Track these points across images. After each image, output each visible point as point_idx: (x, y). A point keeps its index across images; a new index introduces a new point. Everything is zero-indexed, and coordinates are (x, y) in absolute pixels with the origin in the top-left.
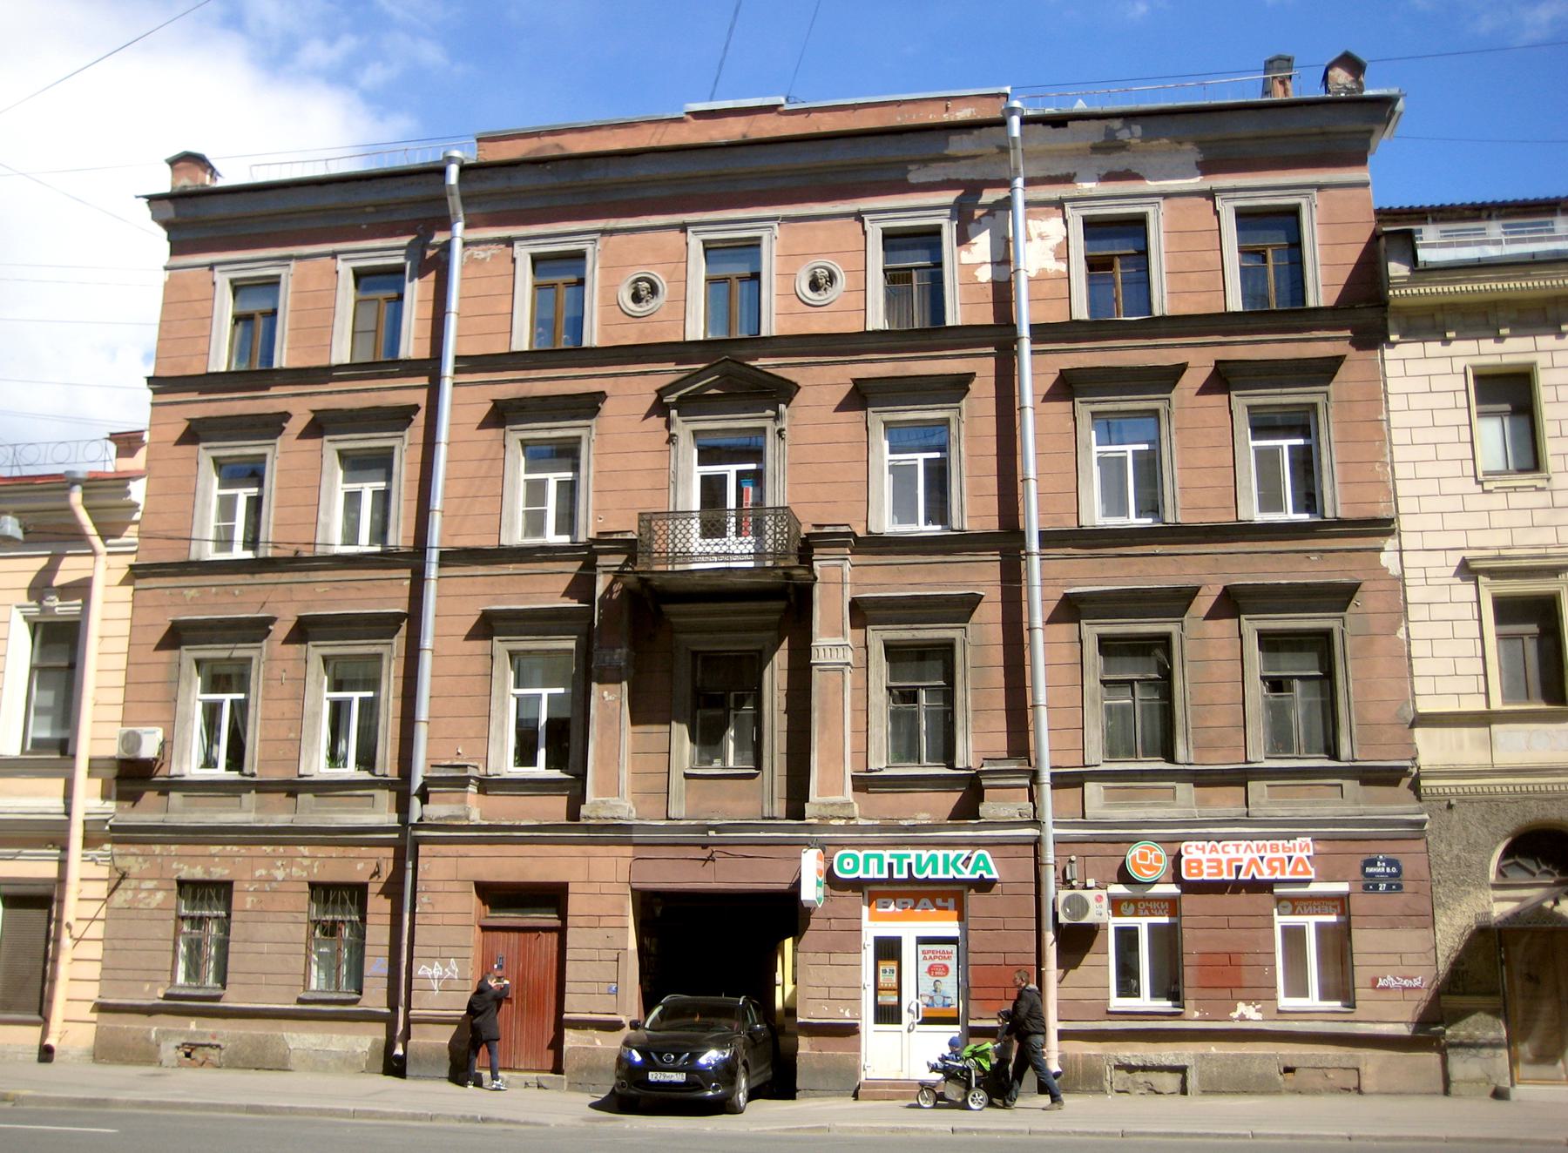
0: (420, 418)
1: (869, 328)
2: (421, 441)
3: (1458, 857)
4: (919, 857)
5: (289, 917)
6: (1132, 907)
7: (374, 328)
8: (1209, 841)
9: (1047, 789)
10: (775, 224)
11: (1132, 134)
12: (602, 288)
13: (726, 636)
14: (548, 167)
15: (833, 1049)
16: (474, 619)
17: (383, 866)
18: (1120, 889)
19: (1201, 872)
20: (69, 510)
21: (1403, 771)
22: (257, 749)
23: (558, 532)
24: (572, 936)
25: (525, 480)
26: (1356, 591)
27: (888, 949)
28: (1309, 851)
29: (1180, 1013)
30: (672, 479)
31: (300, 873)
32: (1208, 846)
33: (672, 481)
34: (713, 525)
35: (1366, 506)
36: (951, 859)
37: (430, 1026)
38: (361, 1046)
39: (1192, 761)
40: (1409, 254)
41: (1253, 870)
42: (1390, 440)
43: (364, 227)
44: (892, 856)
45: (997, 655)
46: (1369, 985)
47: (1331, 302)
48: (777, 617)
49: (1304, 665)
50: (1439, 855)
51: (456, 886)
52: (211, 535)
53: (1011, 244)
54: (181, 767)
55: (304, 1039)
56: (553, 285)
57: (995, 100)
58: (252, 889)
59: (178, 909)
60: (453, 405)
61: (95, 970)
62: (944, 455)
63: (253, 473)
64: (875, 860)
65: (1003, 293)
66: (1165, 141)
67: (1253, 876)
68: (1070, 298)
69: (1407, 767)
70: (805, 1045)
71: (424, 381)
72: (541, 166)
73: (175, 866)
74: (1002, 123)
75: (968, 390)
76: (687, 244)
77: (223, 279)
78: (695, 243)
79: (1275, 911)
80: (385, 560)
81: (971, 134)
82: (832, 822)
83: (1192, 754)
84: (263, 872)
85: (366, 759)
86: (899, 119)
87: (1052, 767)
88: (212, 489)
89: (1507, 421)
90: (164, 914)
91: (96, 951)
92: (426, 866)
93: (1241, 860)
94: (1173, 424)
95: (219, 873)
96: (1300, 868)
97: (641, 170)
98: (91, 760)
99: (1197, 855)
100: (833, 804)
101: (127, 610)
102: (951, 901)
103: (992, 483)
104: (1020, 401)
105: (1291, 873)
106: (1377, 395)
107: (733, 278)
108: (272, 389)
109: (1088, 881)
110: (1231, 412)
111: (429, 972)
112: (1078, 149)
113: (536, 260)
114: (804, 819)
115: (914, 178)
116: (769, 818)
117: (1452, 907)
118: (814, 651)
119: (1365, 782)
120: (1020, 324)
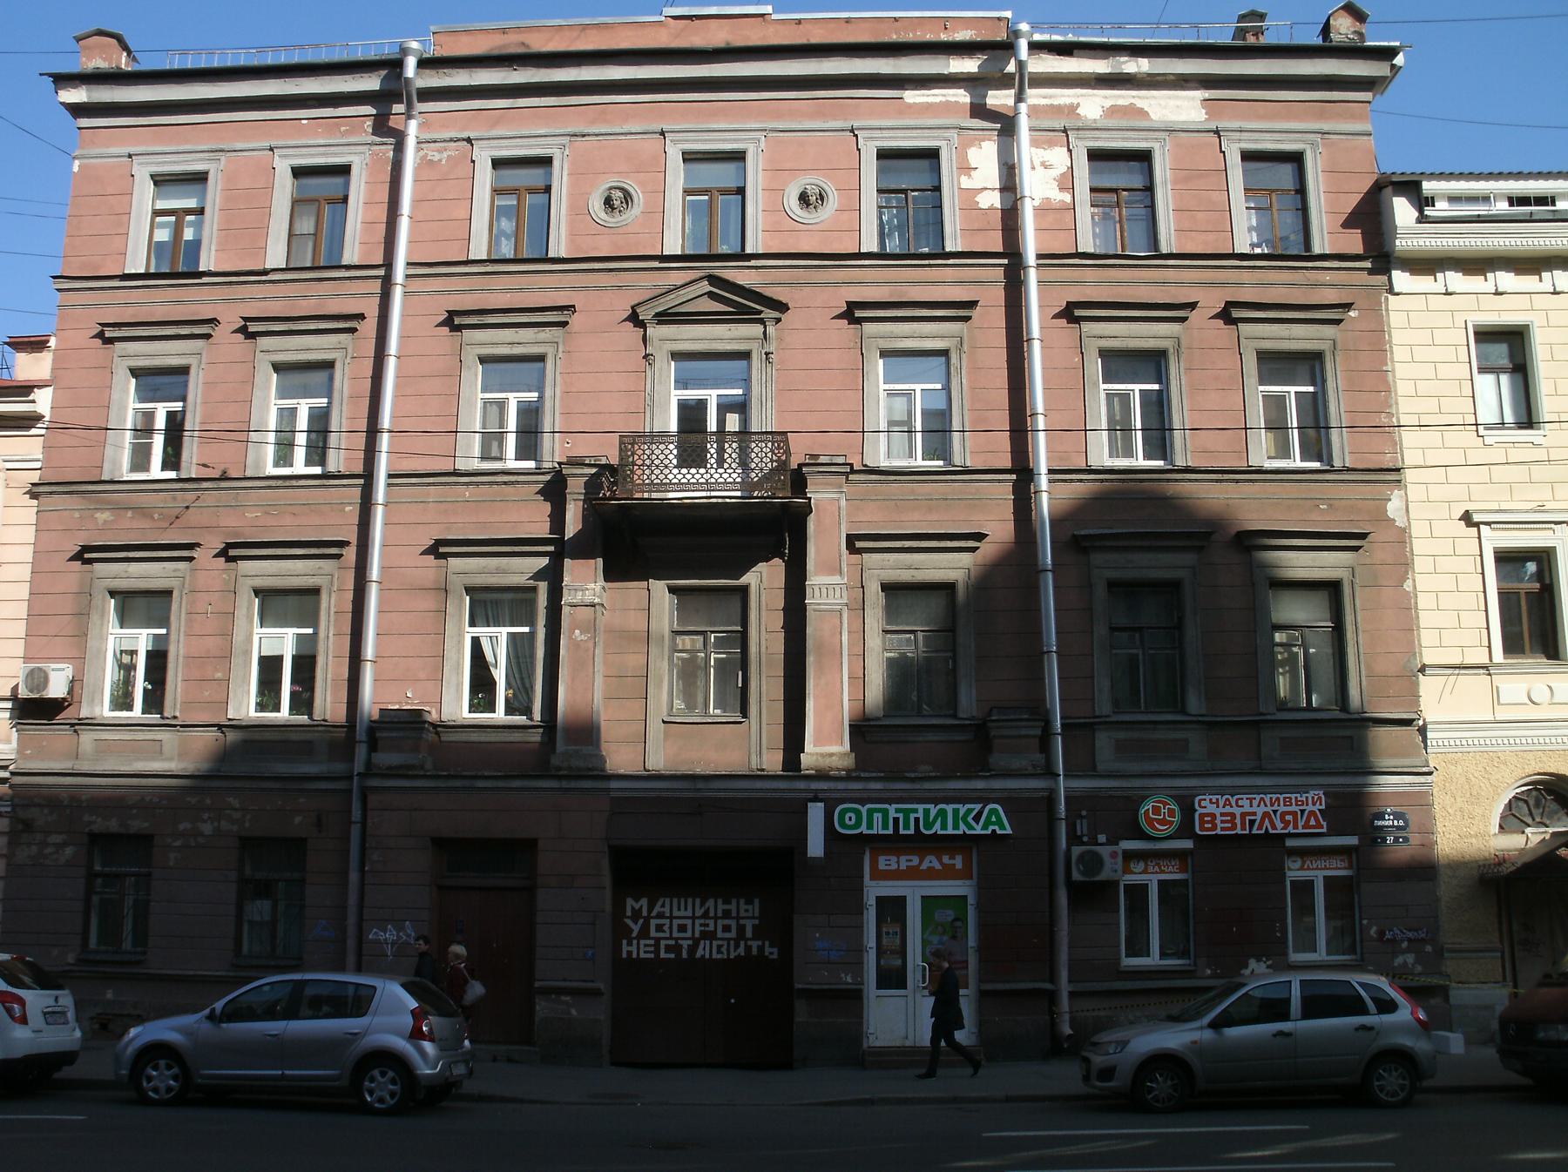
4: (927, 812)
8: (1232, 796)
19: (1215, 827)
22: (179, 690)
28: (1321, 804)
30: (648, 402)
33: (648, 404)
44: (897, 811)
64: (880, 815)
70: (802, 1013)
75: (1146, 112)
86: (895, 37)
89: (1504, 378)
93: (1254, 814)
94: (1182, 364)
96: (1312, 822)
99: (1211, 809)
104: (1027, 334)
105: (1304, 827)
111: (382, 936)
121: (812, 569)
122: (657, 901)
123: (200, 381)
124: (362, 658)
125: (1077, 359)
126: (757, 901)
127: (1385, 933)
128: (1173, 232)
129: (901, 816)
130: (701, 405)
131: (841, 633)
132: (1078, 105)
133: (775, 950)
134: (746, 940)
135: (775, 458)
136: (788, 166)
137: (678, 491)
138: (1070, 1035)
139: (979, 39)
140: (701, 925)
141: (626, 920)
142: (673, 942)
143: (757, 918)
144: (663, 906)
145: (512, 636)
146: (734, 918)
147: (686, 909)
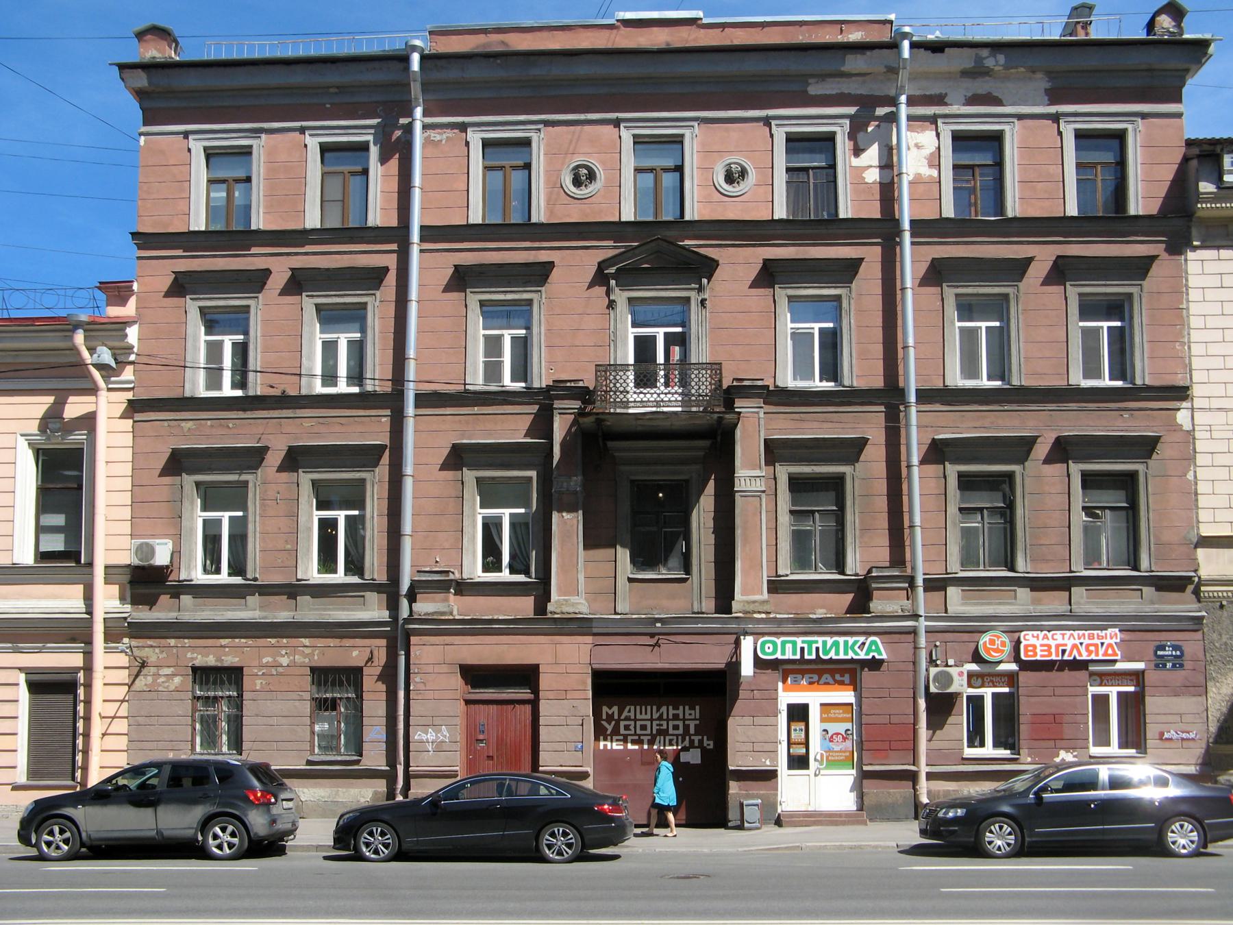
0: (391, 279)
1: (776, 217)
2: (394, 298)
3: (1226, 644)
4: (825, 643)
5: (294, 696)
6: (980, 680)
7: (341, 198)
8: (1042, 631)
9: (920, 590)
10: (696, 124)
11: (995, 62)
12: (546, 172)
13: (659, 468)
14: (499, 61)
15: (759, 788)
16: (446, 452)
17: (375, 653)
18: (974, 667)
19: (1035, 654)
20: (74, 350)
21: (1189, 579)
23: (514, 379)
24: (543, 705)
25: (205, 341)
26: (1158, 442)
27: (799, 713)
28: (1117, 638)
29: (1017, 759)
30: (612, 338)
31: (302, 660)
32: (1041, 634)
33: (613, 340)
34: (645, 376)
35: (1168, 377)
36: (850, 644)
37: (428, 780)
38: (363, 797)
39: (1029, 570)
40: (1216, 174)
41: (1075, 652)
42: (1189, 325)
43: (328, 106)
44: (803, 642)
45: (882, 486)
46: (1157, 737)
47: (1153, 209)
48: (703, 453)
49: (1116, 498)
50: (1212, 642)
51: (445, 669)
52: (318, 370)
53: (895, 151)
54: (189, 573)
55: (315, 793)
56: (502, 168)
57: (881, 26)
58: (260, 673)
59: (193, 691)
60: (421, 268)
61: (122, 743)
62: (685, 330)
63: (237, 320)
65: (888, 192)
66: (1022, 69)
67: (1075, 657)
68: (940, 199)
69: (1192, 577)
71: (394, 247)
72: (492, 60)
73: (189, 655)
74: (894, 46)
76: (620, 137)
77: (197, 147)
78: (627, 135)
79: (1089, 684)
80: (364, 400)
81: (864, 54)
82: (756, 616)
83: (1029, 565)
84: (270, 659)
85: (355, 565)
86: (801, 38)
87: (924, 574)
88: (200, 338)
90: (182, 696)
91: (121, 726)
92: (418, 653)
93: (1066, 645)
94: (1020, 306)
95: (230, 660)
96: (1110, 651)
97: (582, 69)
98: (106, 567)
99: (1033, 641)
100: (754, 602)
101: (128, 439)
102: (847, 678)
103: (878, 350)
105: (1103, 655)
106: (1179, 289)
107: (658, 169)
108: (253, 249)
109: (949, 661)
110: (1066, 298)
111: (424, 737)
112: (950, 73)
113: (487, 144)
114: (731, 613)
115: (814, 89)
116: (698, 613)
117: (1220, 680)
118: (736, 481)
119: (1159, 588)
120: (903, 221)
121: (739, 465)
122: (625, 708)
123: (259, 319)
124: (402, 533)
125: (939, 303)
126: (697, 708)
127: (1164, 734)
128: (1017, 199)
129: (806, 646)
130: (652, 339)
131: (761, 513)
132: (946, 94)
133: (711, 743)
134: (690, 735)
135: (713, 382)
136: (715, 148)
137: (641, 407)
138: (927, 804)
139: (868, 40)
140: (657, 725)
141: (602, 722)
142: (637, 738)
143: (697, 720)
144: (629, 711)
145: (347, 517)
146: (681, 720)
147: (646, 714)
